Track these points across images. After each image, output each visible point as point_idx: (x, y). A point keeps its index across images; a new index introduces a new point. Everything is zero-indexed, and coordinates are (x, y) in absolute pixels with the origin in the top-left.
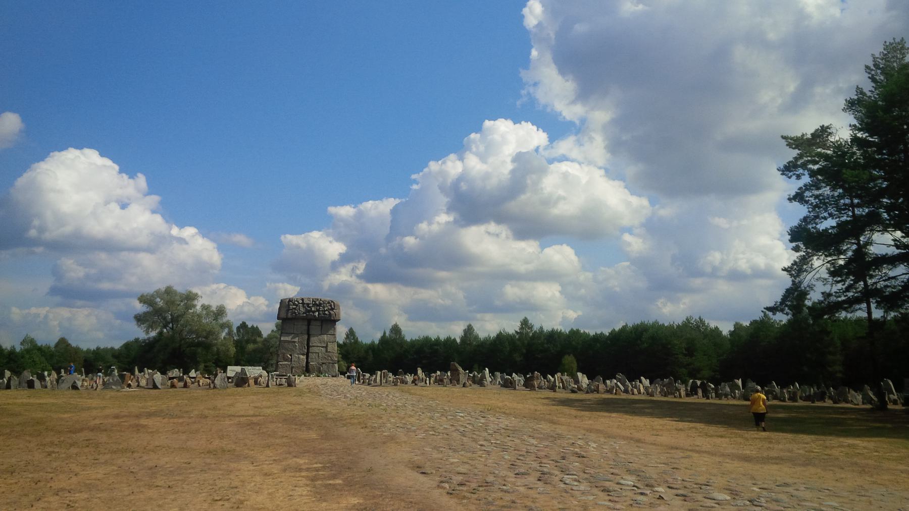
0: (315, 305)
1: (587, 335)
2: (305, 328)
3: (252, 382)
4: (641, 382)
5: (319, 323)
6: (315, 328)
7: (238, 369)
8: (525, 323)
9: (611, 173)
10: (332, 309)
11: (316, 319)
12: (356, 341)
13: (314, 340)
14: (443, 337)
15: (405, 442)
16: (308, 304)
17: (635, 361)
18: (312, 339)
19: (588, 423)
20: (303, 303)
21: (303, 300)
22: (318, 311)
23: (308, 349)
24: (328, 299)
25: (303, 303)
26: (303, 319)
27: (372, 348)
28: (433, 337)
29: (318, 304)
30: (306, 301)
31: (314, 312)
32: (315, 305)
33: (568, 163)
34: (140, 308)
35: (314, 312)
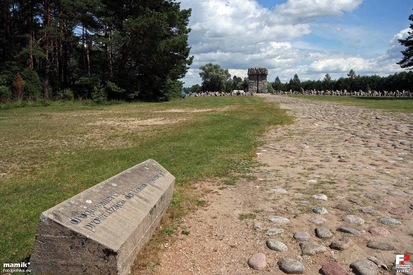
0: (260, 70)
1: (379, 77)
2: (257, 78)
3: (241, 94)
5: (261, 76)
6: (260, 77)
7: (237, 91)
9: (260, 60)
10: (265, 71)
11: (260, 75)
12: (280, 83)
13: (259, 82)
14: (316, 80)
17: (354, 86)
18: (259, 81)
20: (256, 69)
22: (261, 72)
24: (264, 68)
25: (256, 69)
26: (256, 74)
27: (286, 85)
28: (307, 81)
32: (260, 70)
34: (201, 71)
35: (259, 72)
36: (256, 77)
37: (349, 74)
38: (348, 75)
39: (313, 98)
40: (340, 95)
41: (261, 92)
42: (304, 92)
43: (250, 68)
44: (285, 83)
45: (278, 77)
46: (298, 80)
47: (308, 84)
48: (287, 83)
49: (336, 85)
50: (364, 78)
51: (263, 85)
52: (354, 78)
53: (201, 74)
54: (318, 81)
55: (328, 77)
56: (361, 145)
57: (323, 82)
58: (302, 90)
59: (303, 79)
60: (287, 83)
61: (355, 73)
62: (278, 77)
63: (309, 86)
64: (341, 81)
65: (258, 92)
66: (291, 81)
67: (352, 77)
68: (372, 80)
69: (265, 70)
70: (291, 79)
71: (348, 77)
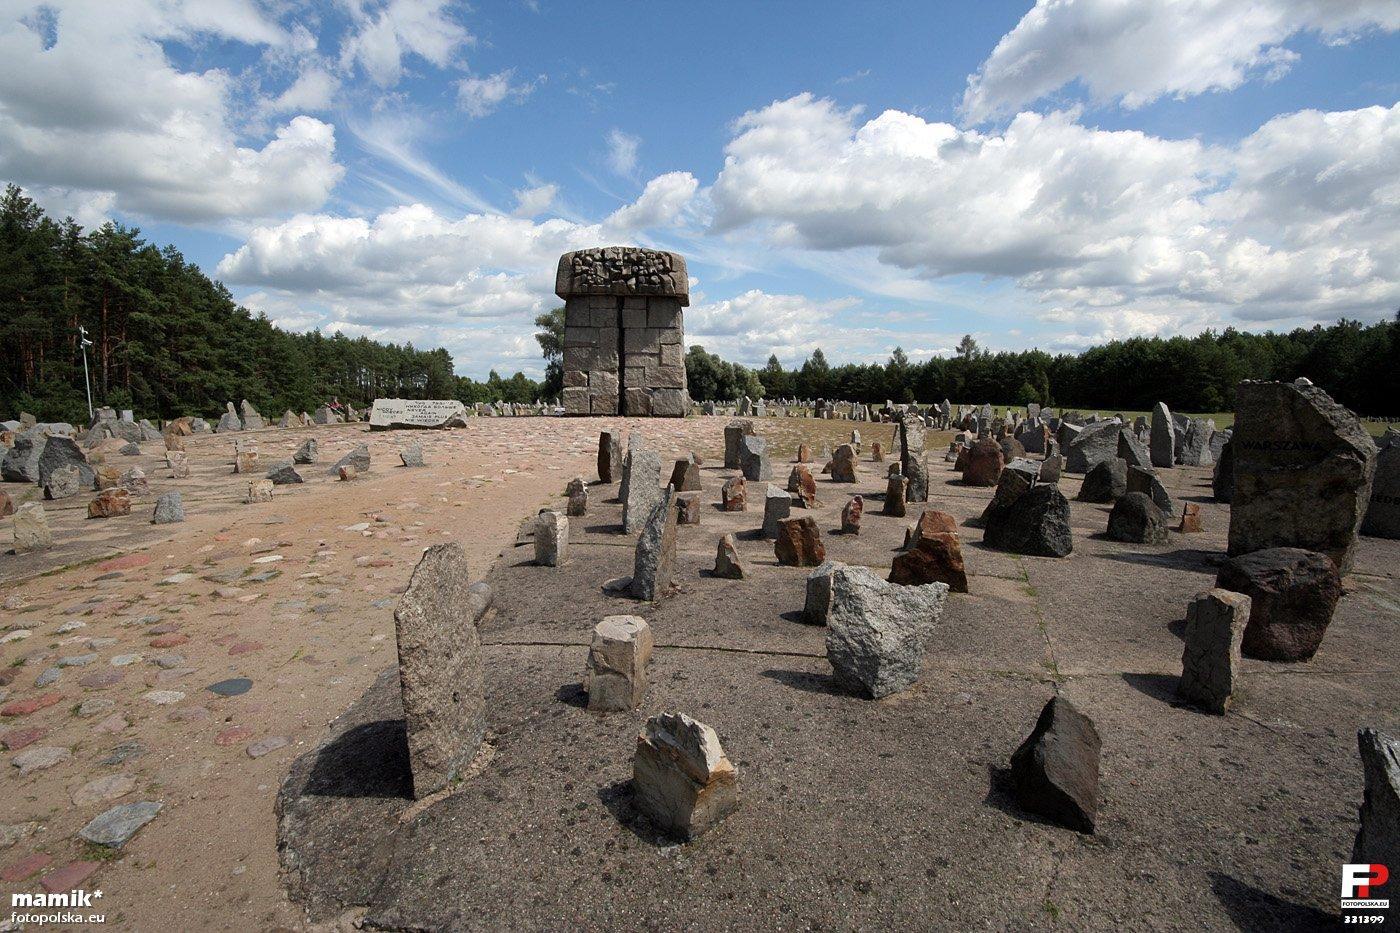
0: (629, 262)
5: (642, 304)
6: (634, 316)
8: (967, 342)
10: (666, 271)
11: (634, 295)
12: (780, 370)
16: (613, 261)
20: (603, 260)
22: (636, 275)
26: (608, 295)
31: (627, 278)
35: (627, 278)
36: (607, 311)
37: (960, 346)
38: (958, 350)
41: (641, 410)
44: (792, 370)
45: (774, 356)
46: (823, 363)
50: (1001, 358)
51: (654, 361)
52: (972, 358)
53: (540, 338)
55: (899, 355)
61: (976, 344)
62: (774, 356)
64: (935, 366)
67: (968, 356)
68: (1028, 363)
69: (667, 264)
71: (956, 355)
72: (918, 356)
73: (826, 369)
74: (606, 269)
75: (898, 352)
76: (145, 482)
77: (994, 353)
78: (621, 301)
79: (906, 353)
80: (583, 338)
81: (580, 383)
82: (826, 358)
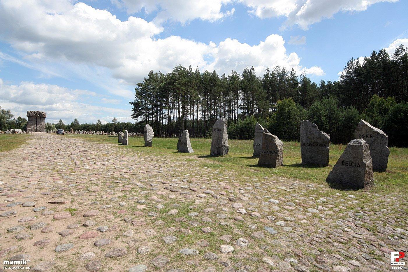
4: (102, 132)
5: (39, 118)
6: (38, 119)
8: (115, 119)
10: (43, 114)
11: (38, 117)
15: (268, 121)
16: (36, 113)
19: (183, 158)
20: (34, 112)
21: (34, 111)
23: (36, 125)
29: (39, 113)
30: (35, 112)
31: (38, 115)
33: (255, 212)
35: (38, 115)
36: (34, 119)
38: (113, 121)
39: (80, 137)
40: (99, 134)
42: (73, 131)
43: (29, 110)
44: (68, 125)
46: (77, 123)
47: (85, 126)
48: (69, 125)
49: (105, 128)
50: (122, 123)
54: (93, 125)
56: (146, 172)
57: (96, 125)
58: (72, 130)
59: (81, 123)
60: (69, 125)
63: (87, 128)
65: (36, 131)
66: (72, 123)
67: (115, 123)
68: (127, 125)
69: (43, 113)
70: (72, 122)
71: (329, 164)
72: (104, 123)
73: (79, 125)
74: (35, 114)
75: (99, 121)
76: (230, 199)
77: (121, 122)
78: (37, 117)
79: (101, 121)
80: (31, 122)
81: (30, 128)
82: (78, 121)
